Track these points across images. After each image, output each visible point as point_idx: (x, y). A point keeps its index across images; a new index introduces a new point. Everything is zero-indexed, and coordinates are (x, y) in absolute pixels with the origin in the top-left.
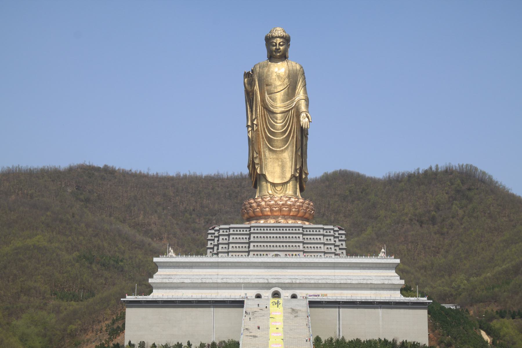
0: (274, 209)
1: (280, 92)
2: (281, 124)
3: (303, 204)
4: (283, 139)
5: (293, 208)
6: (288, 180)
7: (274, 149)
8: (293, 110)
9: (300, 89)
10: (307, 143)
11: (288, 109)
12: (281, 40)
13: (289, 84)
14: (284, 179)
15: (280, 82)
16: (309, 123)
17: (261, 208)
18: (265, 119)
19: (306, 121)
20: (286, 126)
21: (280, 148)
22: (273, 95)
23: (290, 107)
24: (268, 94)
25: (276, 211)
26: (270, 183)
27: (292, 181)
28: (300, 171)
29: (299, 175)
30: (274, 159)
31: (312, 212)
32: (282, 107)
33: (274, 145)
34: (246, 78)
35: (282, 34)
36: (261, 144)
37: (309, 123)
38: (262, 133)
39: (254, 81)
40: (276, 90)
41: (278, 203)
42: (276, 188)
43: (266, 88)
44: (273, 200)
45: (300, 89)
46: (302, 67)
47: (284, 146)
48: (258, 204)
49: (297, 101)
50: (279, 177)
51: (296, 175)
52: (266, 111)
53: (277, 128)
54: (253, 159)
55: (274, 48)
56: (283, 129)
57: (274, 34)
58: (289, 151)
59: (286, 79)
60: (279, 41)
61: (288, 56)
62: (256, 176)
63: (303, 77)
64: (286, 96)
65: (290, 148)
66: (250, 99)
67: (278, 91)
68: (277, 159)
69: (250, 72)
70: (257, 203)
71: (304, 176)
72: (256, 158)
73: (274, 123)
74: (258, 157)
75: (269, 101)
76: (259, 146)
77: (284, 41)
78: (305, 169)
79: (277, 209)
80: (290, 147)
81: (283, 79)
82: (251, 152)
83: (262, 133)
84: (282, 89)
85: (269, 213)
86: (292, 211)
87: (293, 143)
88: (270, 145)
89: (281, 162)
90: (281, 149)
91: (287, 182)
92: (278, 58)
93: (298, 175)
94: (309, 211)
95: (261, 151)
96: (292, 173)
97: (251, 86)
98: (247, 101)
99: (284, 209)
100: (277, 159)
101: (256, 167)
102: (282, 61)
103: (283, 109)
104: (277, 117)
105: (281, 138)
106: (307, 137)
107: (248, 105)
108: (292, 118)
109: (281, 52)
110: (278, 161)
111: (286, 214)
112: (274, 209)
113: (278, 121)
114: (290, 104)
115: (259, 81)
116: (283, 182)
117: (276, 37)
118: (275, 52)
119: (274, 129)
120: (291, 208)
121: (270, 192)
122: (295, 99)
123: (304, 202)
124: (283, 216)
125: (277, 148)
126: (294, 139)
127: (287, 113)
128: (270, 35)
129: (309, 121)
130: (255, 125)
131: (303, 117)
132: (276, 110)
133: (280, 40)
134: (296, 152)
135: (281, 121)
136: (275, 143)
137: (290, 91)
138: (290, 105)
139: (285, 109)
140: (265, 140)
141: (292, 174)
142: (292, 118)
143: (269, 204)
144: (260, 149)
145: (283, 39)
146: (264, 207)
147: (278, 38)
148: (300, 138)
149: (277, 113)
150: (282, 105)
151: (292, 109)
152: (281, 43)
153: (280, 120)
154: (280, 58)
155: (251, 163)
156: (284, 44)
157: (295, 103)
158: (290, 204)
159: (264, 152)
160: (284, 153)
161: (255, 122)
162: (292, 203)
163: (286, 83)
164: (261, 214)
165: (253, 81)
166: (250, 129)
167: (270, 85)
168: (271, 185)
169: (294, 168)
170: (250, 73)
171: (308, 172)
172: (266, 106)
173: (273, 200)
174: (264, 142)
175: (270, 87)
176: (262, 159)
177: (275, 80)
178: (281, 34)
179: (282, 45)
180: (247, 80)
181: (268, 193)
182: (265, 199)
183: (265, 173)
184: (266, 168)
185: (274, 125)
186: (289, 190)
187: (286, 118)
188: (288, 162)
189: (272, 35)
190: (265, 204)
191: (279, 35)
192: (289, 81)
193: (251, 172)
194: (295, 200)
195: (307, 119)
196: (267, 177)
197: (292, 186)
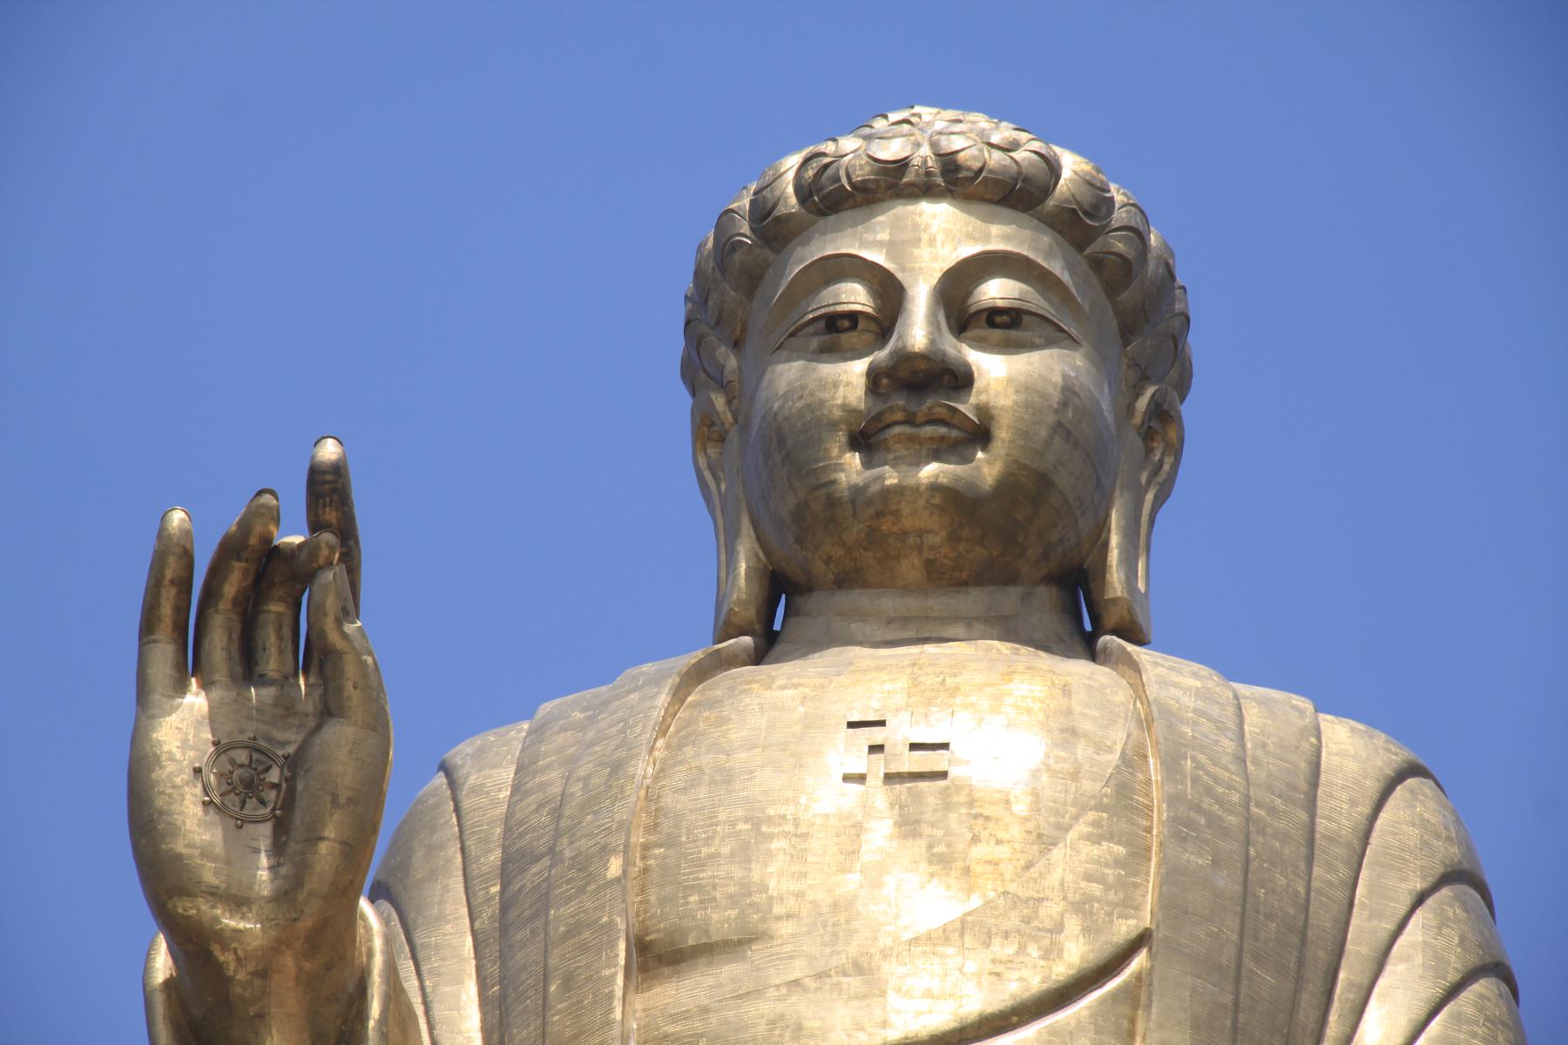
13: (1141, 941)
34: (191, 665)
39: (353, 697)
59: (1082, 828)
77: (1056, 267)
81: (1016, 832)
92: (940, 577)
97: (281, 827)
133: (987, 238)
147: (925, 190)
152: (996, 291)
167: (711, 950)
171: (955, 920)
175: (727, 972)
180: (213, 718)
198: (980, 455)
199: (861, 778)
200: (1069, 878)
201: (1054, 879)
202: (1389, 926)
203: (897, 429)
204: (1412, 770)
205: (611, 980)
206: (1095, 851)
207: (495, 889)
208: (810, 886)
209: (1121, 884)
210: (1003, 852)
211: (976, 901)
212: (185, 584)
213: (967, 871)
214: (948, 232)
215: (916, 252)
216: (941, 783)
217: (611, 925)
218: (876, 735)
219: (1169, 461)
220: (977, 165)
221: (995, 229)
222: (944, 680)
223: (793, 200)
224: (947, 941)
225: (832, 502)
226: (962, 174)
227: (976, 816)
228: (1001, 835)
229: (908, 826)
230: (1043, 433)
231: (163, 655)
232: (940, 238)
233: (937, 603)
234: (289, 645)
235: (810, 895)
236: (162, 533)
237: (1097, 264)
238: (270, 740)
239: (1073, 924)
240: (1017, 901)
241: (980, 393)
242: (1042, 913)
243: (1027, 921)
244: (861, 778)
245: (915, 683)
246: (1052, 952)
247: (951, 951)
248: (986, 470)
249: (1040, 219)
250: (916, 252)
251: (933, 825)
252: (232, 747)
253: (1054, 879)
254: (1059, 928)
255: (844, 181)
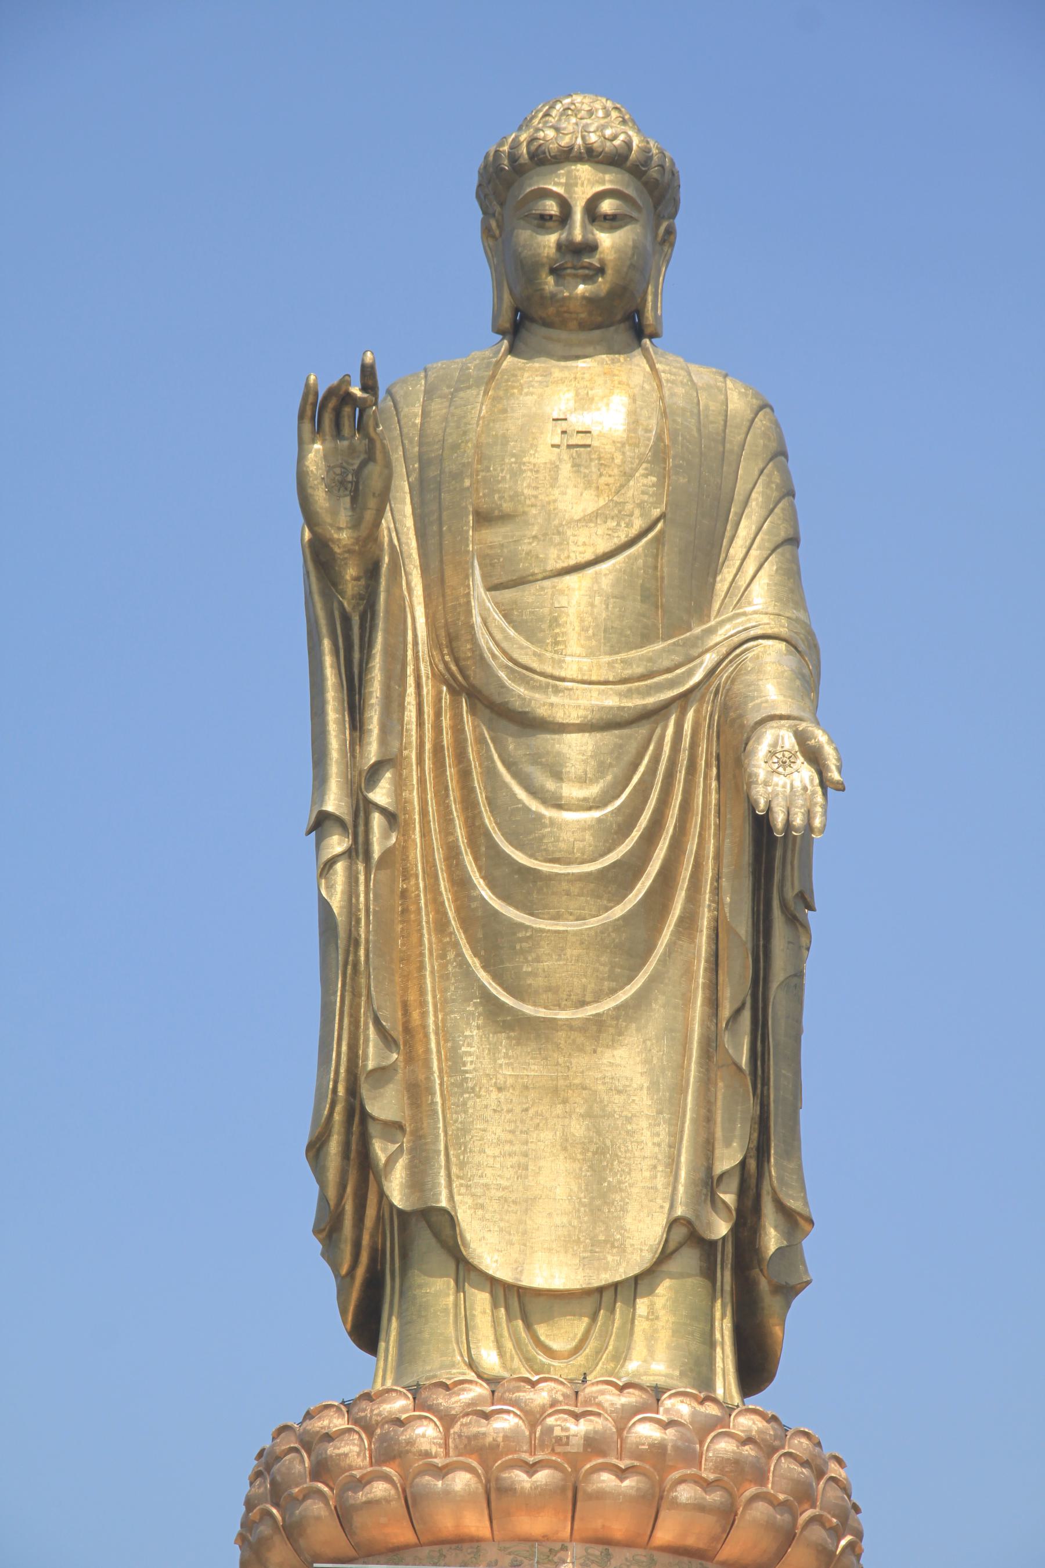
0: (519, 1476)
1: (591, 571)
2: (590, 809)
3: (769, 1456)
4: (604, 928)
5: (682, 1481)
6: (646, 1265)
7: (528, 1009)
8: (690, 715)
9: (750, 567)
10: (799, 975)
11: (651, 700)
12: (609, 180)
13: (663, 516)
14: (610, 1258)
15: (589, 495)
16: (825, 794)
17: (403, 1477)
18: (465, 775)
19: (798, 785)
20: (636, 834)
21: (583, 1004)
22: (527, 595)
23: (672, 684)
24: (491, 588)
25: (536, 1501)
26: (493, 1283)
27: (671, 1276)
28: (742, 1194)
29: (735, 1230)
30: (532, 1094)
31: (843, 1543)
32: (606, 683)
33: (534, 974)
34: (318, 431)
35: (615, 137)
36: (421, 967)
37: (819, 798)
38: (433, 888)
39: (379, 456)
40: (553, 553)
41: (557, 1432)
42: (542, 1330)
43: (475, 539)
44: (515, 1403)
45: (750, 567)
46: (794, 496)
47: (613, 991)
48: (384, 1438)
49: (724, 650)
50: (569, 1242)
51: (709, 1225)
52: (472, 710)
53: (562, 845)
54: (353, 1091)
55: (552, 239)
56: (603, 855)
57: (550, 134)
58: (651, 1030)
59: (641, 471)
60: (593, 184)
61: (657, 318)
62: (373, 1236)
63: (777, 478)
64: (638, 605)
65: (658, 1012)
66: (346, 619)
67: (572, 562)
68: (555, 1091)
69: (345, 381)
70: (370, 1434)
71: (772, 1240)
72: (382, 1074)
73: (534, 805)
74: (399, 1076)
75: (499, 636)
76: (405, 989)
77: (630, 191)
78: (781, 1179)
79: (543, 1476)
80: (662, 999)
81: (616, 471)
82: (341, 1028)
83: (433, 888)
84: (603, 546)
85: (475, 1523)
86: (675, 1504)
87: (688, 973)
88: (497, 977)
89: (588, 1115)
90: (590, 1011)
91: (637, 1278)
92: (583, 326)
93: (722, 1228)
94: (812, 1520)
95: (424, 1026)
96: (672, 1207)
97: (354, 500)
98: (324, 630)
99: (607, 1480)
100: (555, 1091)
101: (381, 1150)
102: (610, 351)
103: (611, 700)
104: (559, 754)
105: (594, 922)
106: (796, 923)
107: (328, 660)
108: (681, 776)
109: (601, 271)
110: (559, 1109)
111: (619, 1527)
112: (519, 1476)
113: (571, 791)
114: (666, 663)
115: (421, 491)
116: (596, 1283)
117: (567, 156)
118: (553, 271)
119: (532, 856)
120: (662, 1481)
121: (489, 1359)
122: (712, 631)
123: (776, 1437)
124: (596, 1550)
125: (560, 1007)
126: (692, 939)
127: (641, 731)
128: (516, 145)
129: (824, 783)
130: (377, 819)
131: (772, 753)
132: (554, 699)
133: (603, 183)
134: (710, 1046)
135: (593, 790)
136: (538, 960)
137: (668, 564)
138: (669, 670)
139: (629, 694)
140: (456, 945)
141: (679, 1211)
142: (681, 776)
143: (476, 1436)
144: (415, 1015)
145: (626, 176)
146: (435, 1466)
147: (579, 159)
148: (743, 928)
149: (562, 728)
150: (601, 666)
151: (685, 697)
152: (607, 206)
153: (583, 780)
154: (599, 327)
155: (337, 1117)
156: (634, 214)
157: (709, 660)
158: (652, 1446)
159: (446, 1033)
160: (612, 1045)
161: (381, 795)
162: (671, 1433)
163: (641, 505)
164: (403, 1535)
165: (370, 457)
166: (337, 844)
167: (505, 518)
168: (495, 1305)
169: (693, 1169)
170: (348, 398)
171: (806, 1204)
172: (470, 673)
173: (515, 1403)
174: (451, 955)
176: (433, 1094)
177: (555, 479)
178: (608, 132)
179: (612, 222)
180: (325, 457)
181: (472, 1365)
182: (442, 1400)
183: (451, 1198)
184: (462, 1165)
185: (539, 817)
186: (651, 1352)
187: (635, 766)
188: (644, 1123)
189: (532, 140)
190: (446, 1436)
191: (593, 138)
192: (659, 484)
193: (332, 1193)
194: (694, 1414)
195: (805, 774)
196: (468, 1236)
197: (672, 1319)
198: (600, 279)
199: (558, 446)
200: (636, 493)
201: (630, 493)
202: (751, 486)
203: (569, 271)
204: (761, 408)
205: (468, 531)
206: (645, 481)
207: (416, 465)
208: (540, 494)
209: (654, 494)
210: (611, 480)
211: (602, 502)
212: (314, 404)
213: (598, 488)
214: (589, 180)
215: (576, 189)
216: (589, 449)
217: (466, 508)
218: (564, 425)
219: (670, 251)
220: (600, 150)
221: (607, 177)
222: (588, 393)
223: (526, 156)
224: (591, 521)
225: (542, 297)
226: (595, 154)
227: (602, 464)
228: (611, 472)
229: (576, 465)
230: (625, 269)
231: (307, 426)
232: (586, 183)
233: (584, 336)
234: (352, 420)
235: (540, 497)
236: (307, 385)
237: (646, 184)
238: (348, 463)
239: (637, 512)
240: (617, 503)
241: (601, 253)
242: (626, 508)
243: (620, 512)
244: (558, 446)
245: (577, 394)
246: (629, 525)
247: (592, 525)
248: (603, 286)
249: (625, 170)
250: (576, 189)
251: (586, 467)
252: (334, 467)
253: (630, 493)
254: (631, 515)
255: (548, 154)
